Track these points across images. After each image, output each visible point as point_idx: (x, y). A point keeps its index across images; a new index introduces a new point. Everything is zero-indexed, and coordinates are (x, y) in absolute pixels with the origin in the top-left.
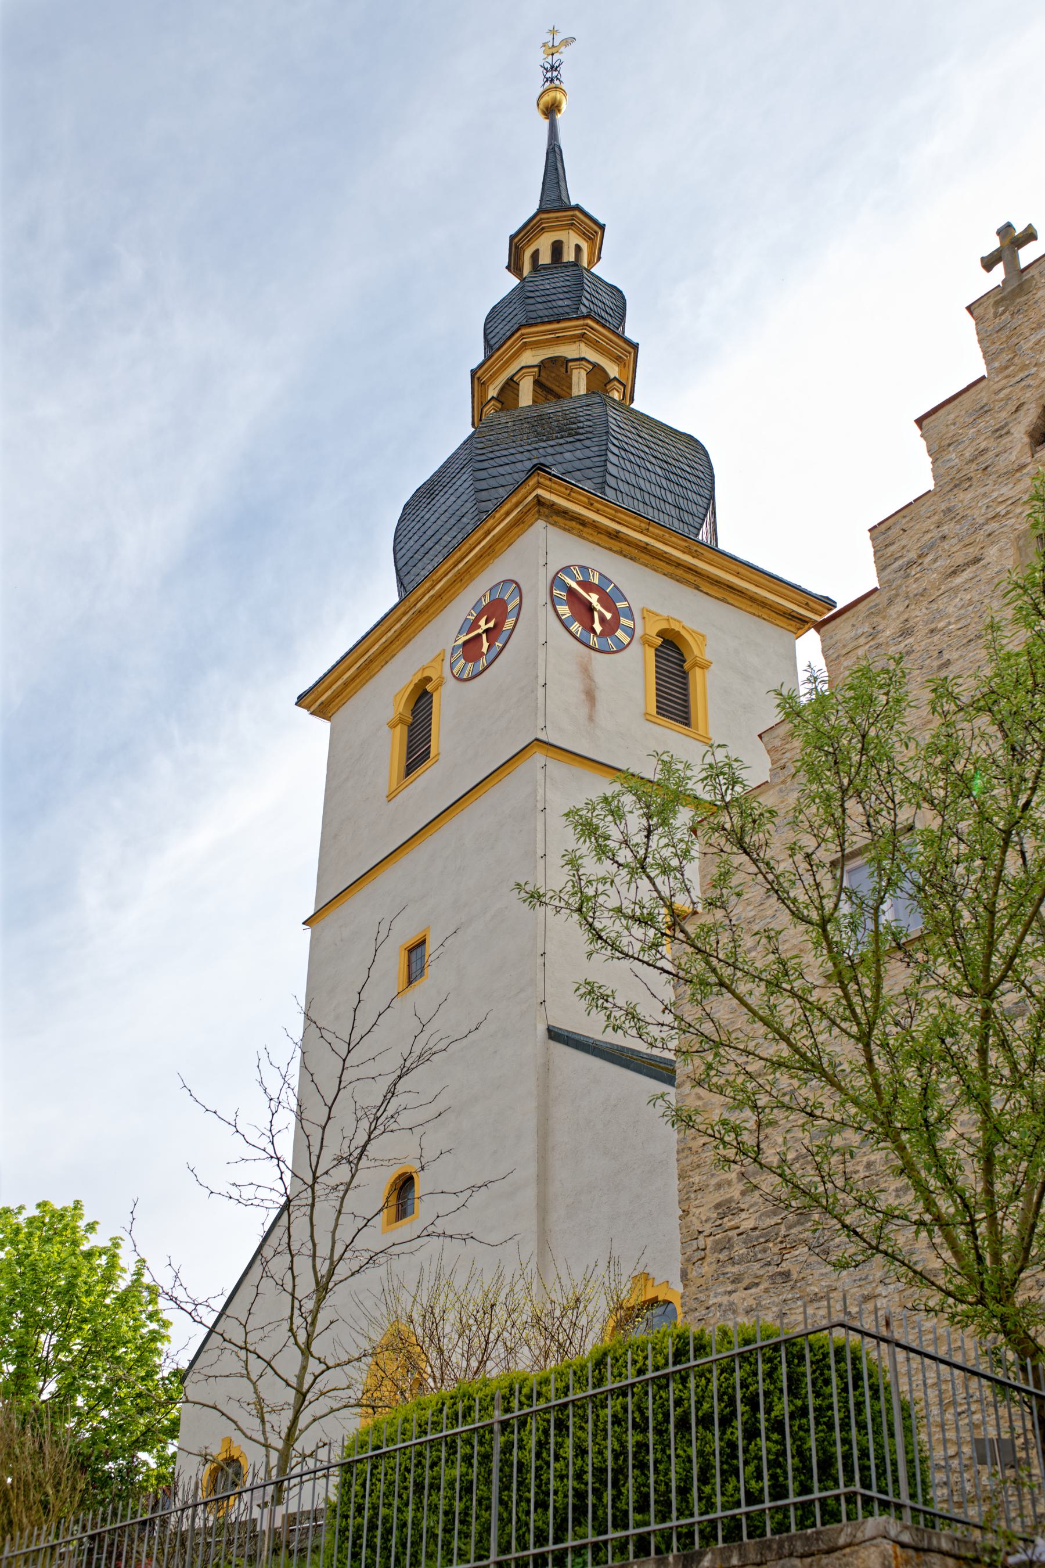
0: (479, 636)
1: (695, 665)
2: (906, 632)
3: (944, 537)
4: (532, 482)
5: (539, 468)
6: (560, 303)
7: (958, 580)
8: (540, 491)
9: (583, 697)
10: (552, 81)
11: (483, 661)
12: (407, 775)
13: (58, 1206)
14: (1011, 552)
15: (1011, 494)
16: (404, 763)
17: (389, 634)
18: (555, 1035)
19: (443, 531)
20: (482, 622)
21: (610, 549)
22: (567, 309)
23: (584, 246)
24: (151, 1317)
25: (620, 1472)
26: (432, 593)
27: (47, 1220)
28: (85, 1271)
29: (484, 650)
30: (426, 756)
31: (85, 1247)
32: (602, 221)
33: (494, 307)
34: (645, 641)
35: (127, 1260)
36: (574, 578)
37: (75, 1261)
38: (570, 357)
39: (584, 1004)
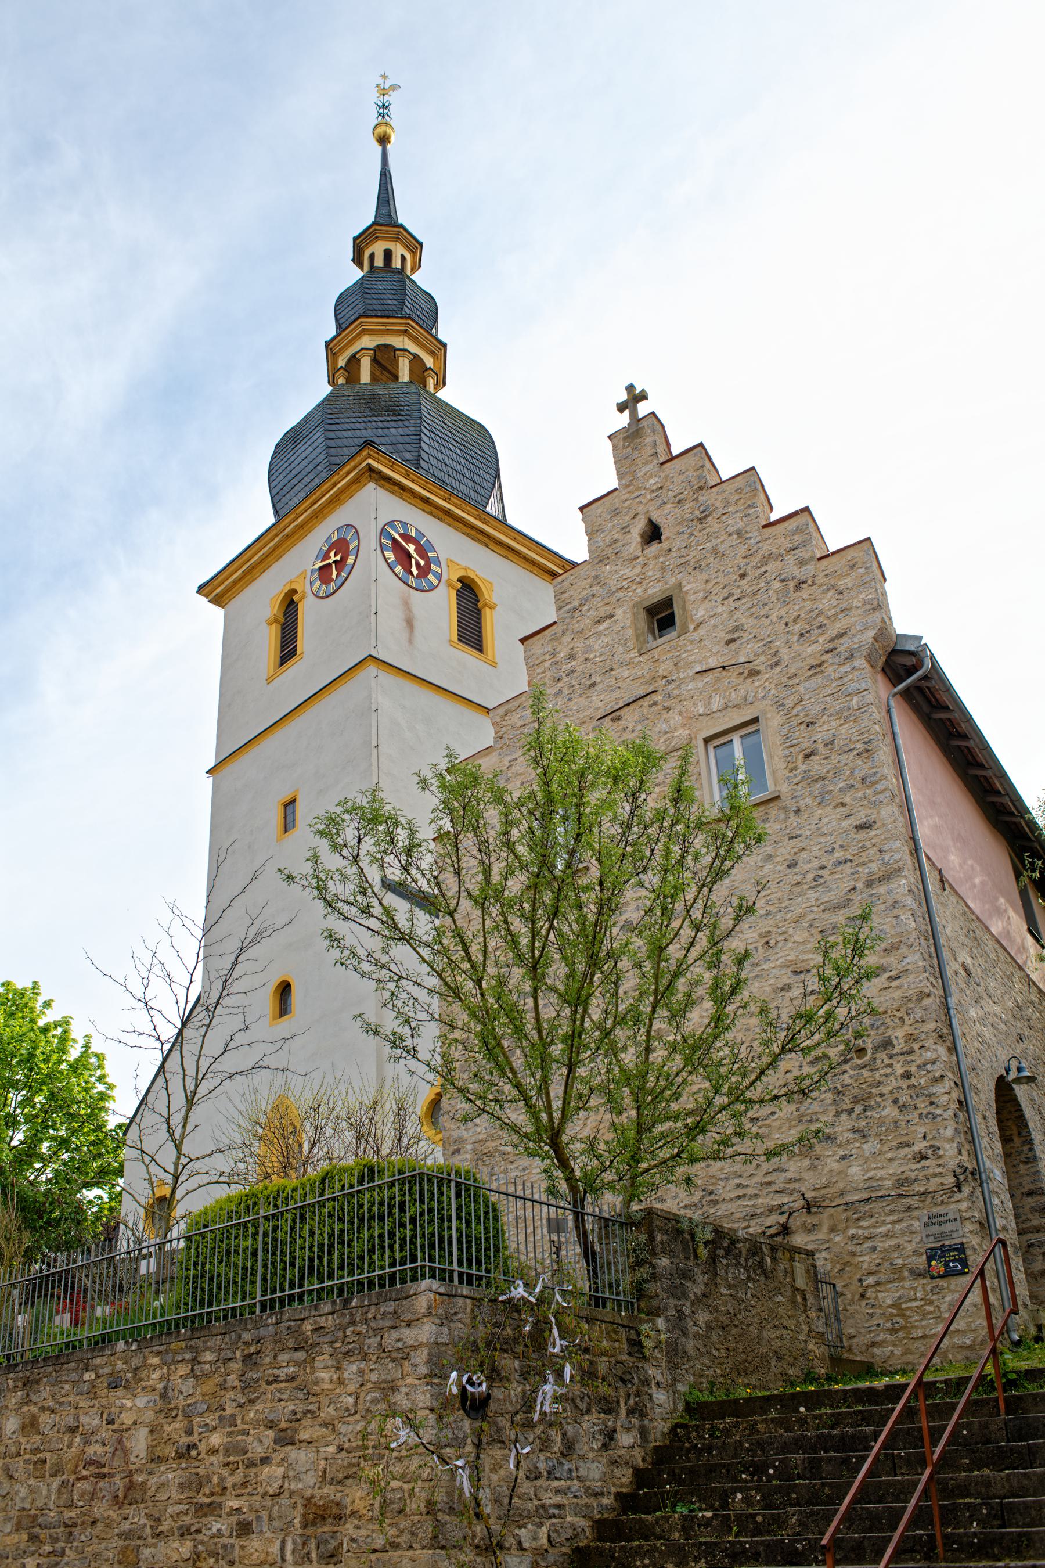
0: (330, 565)
1: (485, 605)
2: (572, 657)
3: (594, 595)
4: (365, 453)
5: (368, 443)
6: (390, 302)
7: (601, 627)
8: (370, 461)
9: (404, 624)
10: (383, 116)
11: (333, 586)
12: (281, 664)
13: (19, 985)
14: (629, 615)
15: (630, 574)
16: (279, 655)
17: (266, 549)
19: (304, 473)
20: (332, 554)
21: (423, 510)
22: (394, 308)
23: (408, 256)
24: (100, 1079)
25: (331, 1246)
26: (296, 523)
27: (10, 997)
28: (43, 1043)
29: (334, 576)
30: (293, 653)
31: (41, 1023)
32: (420, 240)
33: (342, 294)
34: (449, 585)
35: (77, 1032)
36: (396, 530)
37: (33, 1036)
38: (397, 347)
39: (327, 943)
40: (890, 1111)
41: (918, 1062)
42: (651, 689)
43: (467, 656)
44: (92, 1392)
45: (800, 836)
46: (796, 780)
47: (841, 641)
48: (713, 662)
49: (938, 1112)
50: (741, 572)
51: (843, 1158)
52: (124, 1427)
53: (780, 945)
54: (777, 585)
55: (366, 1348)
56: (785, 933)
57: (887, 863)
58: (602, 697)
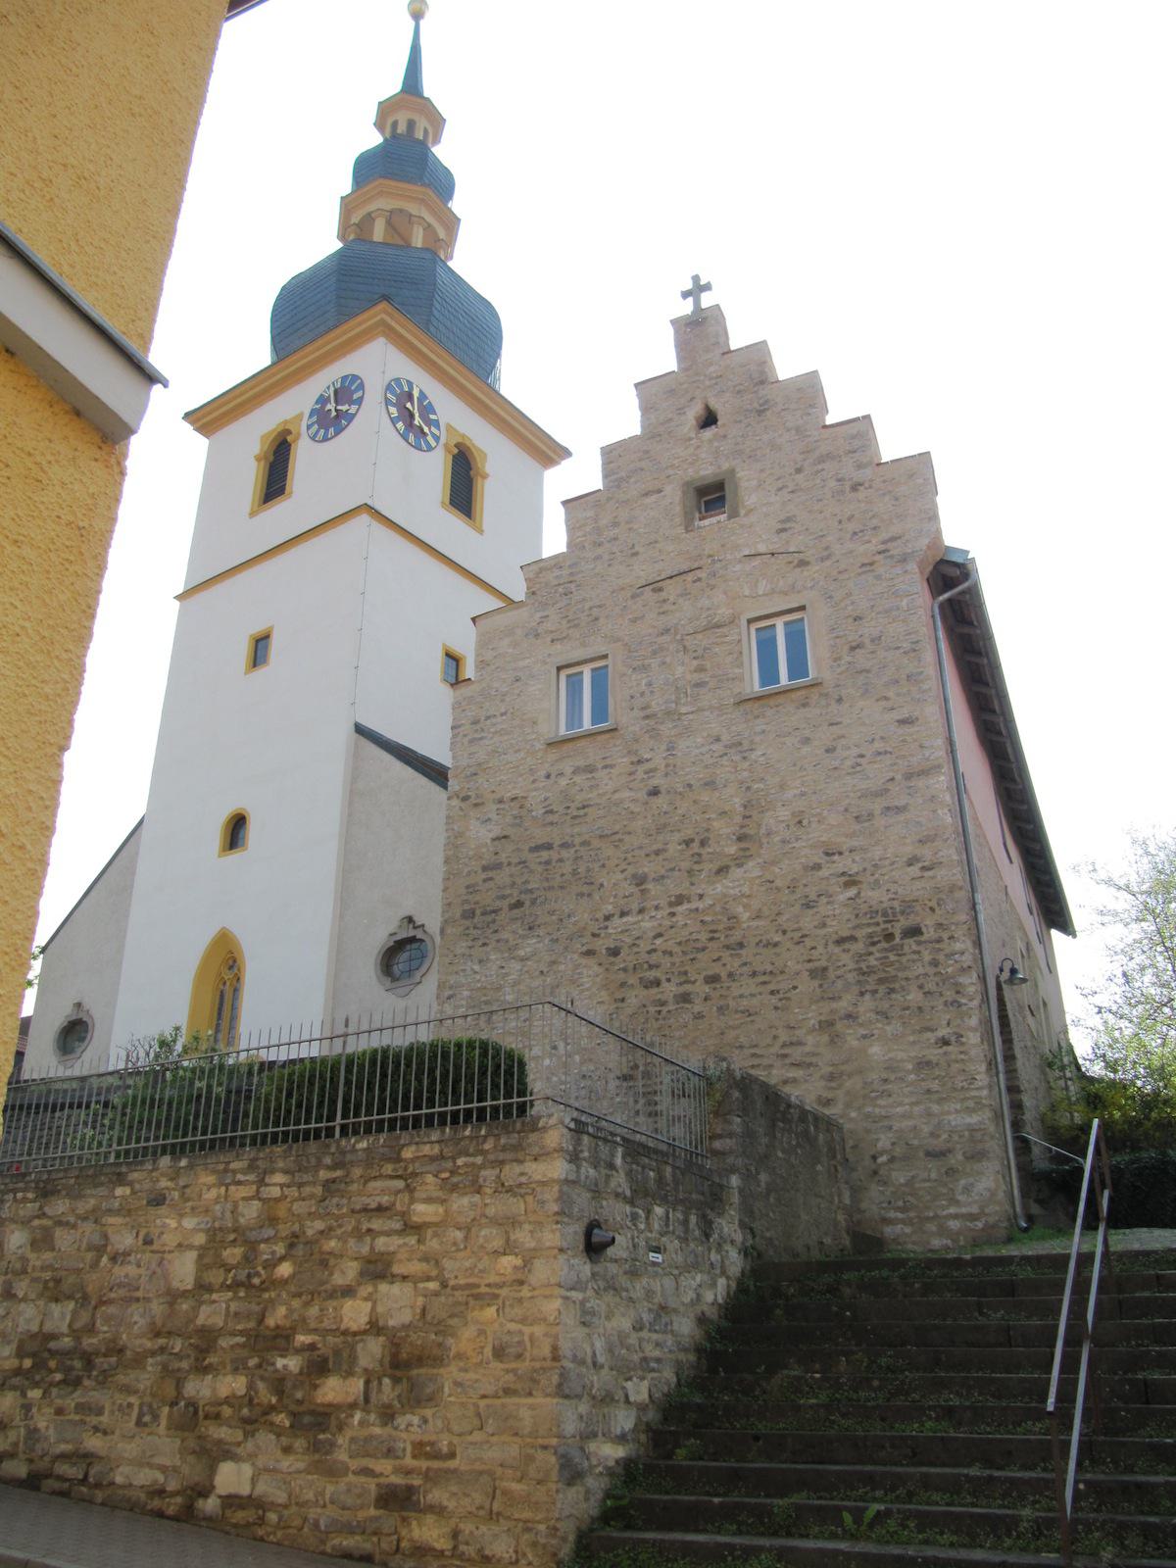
2: (616, 524)
18: (360, 730)
23: (430, 131)
40: (914, 996)
41: (947, 951)
42: (696, 566)
43: (454, 521)
44: (125, 1211)
45: (840, 723)
46: (839, 670)
47: (895, 544)
48: (762, 548)
49: (963, 1001)
50: (798, 466)
51: (864, 1037)
52: (167, 1249)
53: (814, 825)
54: (833, 484)
55: (481, 1180)
56: (820, 814)
57: (928, 759)
58: (644, 567)
